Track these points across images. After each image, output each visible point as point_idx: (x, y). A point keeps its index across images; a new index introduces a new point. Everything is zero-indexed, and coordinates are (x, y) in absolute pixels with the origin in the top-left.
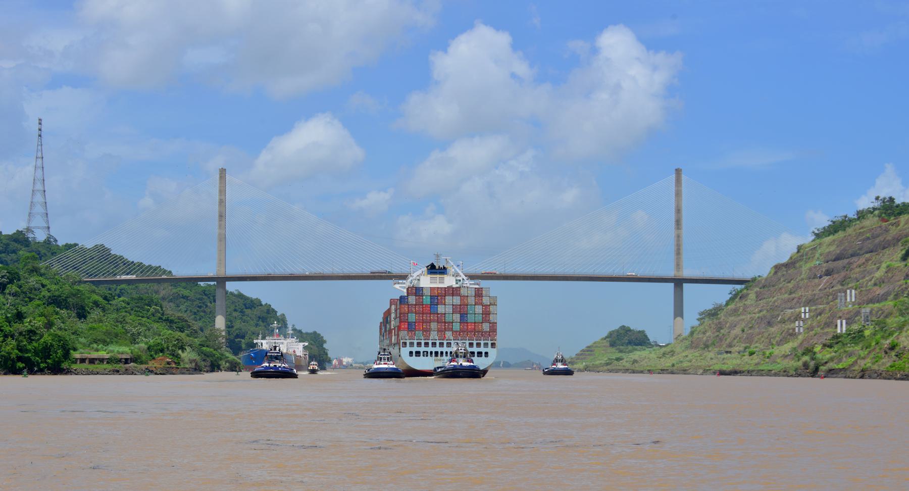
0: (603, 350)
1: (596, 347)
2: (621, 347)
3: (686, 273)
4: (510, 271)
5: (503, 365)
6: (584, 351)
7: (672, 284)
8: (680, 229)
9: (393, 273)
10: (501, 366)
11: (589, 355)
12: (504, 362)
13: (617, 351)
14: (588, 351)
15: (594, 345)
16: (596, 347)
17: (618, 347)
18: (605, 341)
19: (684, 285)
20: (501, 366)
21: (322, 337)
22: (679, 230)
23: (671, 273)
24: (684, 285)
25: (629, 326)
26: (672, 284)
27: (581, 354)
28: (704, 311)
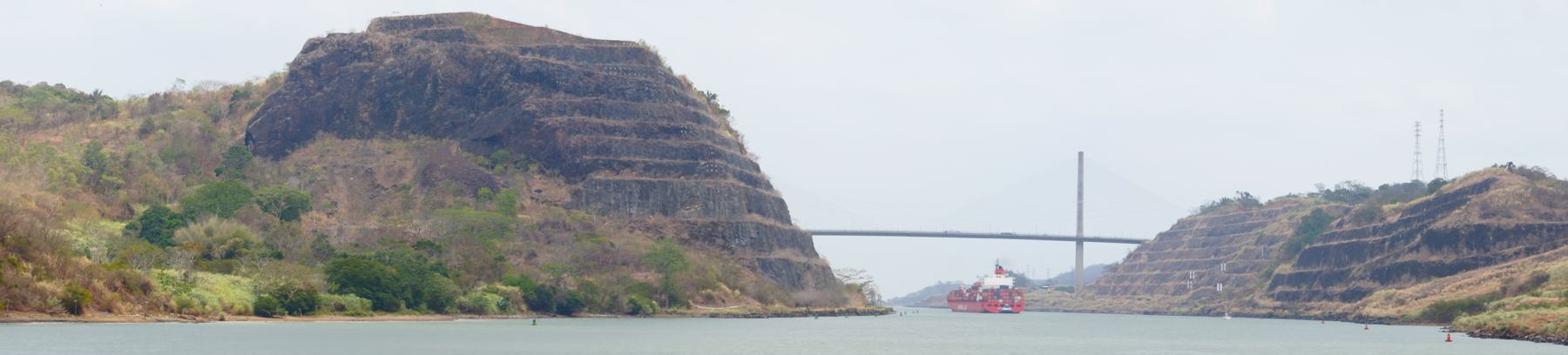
3: (1087, 233)
23: (1073, 233)
26: (1074, 243)
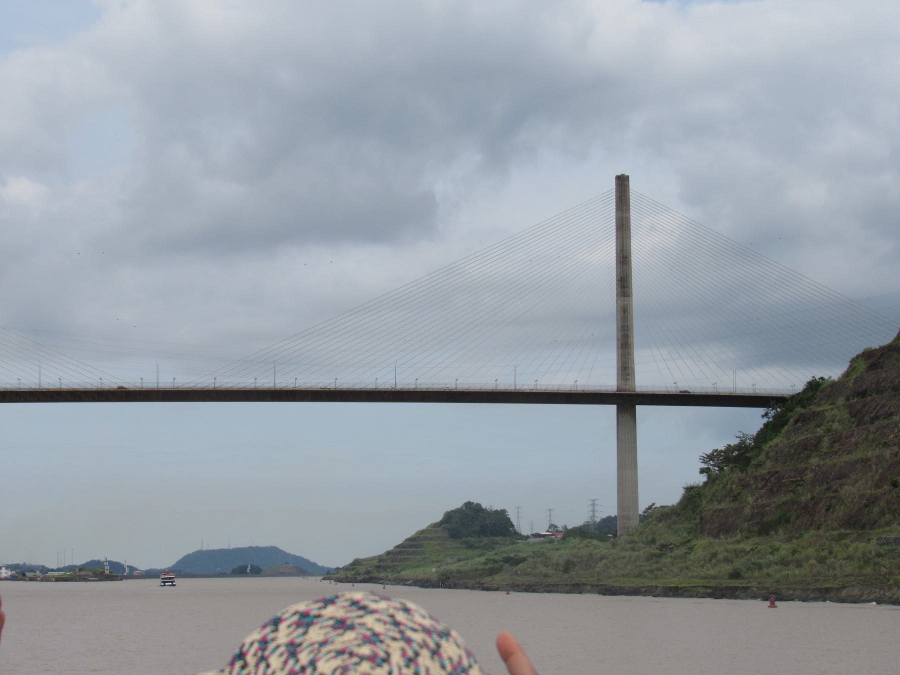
0: (438, 545)
1: (426, 539)
2: (469, 539)
4: (405, 382)
5: (250, 570)
6: (404, 548)
7: (613, 408)
8: (629, 296)
9: (690, 393)
10: (248, 571)
11: (414, 553)
12: (252, 566)
13: (464, 546)
14: (411, 546)
15: (422, 536)
16: (426, 539)
17: (464, 539)
18: (439, 529)
19: (640, 409)
20: (248, 571)
21: (758, 432)
22: (627, 298)
23: (608, 381)
24: (640, 409)
25: (99, 559)
26: (613, 408)
27: (400, 553)
28: (712, 454)
